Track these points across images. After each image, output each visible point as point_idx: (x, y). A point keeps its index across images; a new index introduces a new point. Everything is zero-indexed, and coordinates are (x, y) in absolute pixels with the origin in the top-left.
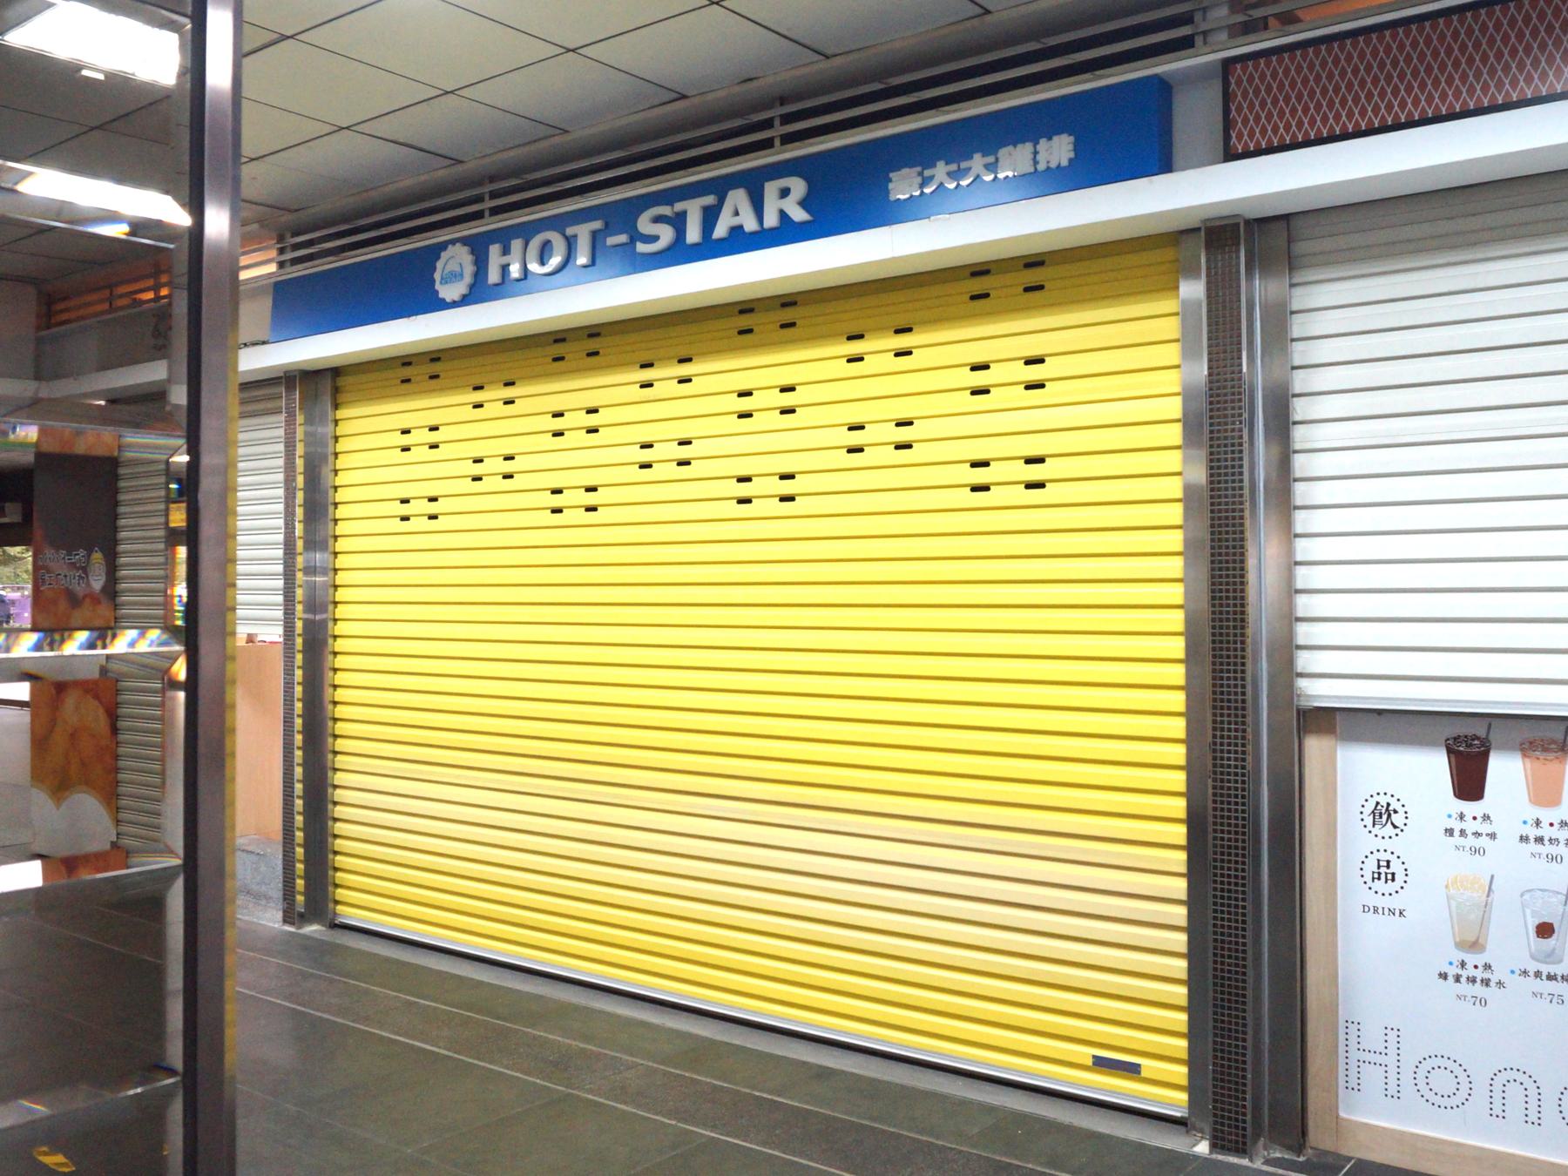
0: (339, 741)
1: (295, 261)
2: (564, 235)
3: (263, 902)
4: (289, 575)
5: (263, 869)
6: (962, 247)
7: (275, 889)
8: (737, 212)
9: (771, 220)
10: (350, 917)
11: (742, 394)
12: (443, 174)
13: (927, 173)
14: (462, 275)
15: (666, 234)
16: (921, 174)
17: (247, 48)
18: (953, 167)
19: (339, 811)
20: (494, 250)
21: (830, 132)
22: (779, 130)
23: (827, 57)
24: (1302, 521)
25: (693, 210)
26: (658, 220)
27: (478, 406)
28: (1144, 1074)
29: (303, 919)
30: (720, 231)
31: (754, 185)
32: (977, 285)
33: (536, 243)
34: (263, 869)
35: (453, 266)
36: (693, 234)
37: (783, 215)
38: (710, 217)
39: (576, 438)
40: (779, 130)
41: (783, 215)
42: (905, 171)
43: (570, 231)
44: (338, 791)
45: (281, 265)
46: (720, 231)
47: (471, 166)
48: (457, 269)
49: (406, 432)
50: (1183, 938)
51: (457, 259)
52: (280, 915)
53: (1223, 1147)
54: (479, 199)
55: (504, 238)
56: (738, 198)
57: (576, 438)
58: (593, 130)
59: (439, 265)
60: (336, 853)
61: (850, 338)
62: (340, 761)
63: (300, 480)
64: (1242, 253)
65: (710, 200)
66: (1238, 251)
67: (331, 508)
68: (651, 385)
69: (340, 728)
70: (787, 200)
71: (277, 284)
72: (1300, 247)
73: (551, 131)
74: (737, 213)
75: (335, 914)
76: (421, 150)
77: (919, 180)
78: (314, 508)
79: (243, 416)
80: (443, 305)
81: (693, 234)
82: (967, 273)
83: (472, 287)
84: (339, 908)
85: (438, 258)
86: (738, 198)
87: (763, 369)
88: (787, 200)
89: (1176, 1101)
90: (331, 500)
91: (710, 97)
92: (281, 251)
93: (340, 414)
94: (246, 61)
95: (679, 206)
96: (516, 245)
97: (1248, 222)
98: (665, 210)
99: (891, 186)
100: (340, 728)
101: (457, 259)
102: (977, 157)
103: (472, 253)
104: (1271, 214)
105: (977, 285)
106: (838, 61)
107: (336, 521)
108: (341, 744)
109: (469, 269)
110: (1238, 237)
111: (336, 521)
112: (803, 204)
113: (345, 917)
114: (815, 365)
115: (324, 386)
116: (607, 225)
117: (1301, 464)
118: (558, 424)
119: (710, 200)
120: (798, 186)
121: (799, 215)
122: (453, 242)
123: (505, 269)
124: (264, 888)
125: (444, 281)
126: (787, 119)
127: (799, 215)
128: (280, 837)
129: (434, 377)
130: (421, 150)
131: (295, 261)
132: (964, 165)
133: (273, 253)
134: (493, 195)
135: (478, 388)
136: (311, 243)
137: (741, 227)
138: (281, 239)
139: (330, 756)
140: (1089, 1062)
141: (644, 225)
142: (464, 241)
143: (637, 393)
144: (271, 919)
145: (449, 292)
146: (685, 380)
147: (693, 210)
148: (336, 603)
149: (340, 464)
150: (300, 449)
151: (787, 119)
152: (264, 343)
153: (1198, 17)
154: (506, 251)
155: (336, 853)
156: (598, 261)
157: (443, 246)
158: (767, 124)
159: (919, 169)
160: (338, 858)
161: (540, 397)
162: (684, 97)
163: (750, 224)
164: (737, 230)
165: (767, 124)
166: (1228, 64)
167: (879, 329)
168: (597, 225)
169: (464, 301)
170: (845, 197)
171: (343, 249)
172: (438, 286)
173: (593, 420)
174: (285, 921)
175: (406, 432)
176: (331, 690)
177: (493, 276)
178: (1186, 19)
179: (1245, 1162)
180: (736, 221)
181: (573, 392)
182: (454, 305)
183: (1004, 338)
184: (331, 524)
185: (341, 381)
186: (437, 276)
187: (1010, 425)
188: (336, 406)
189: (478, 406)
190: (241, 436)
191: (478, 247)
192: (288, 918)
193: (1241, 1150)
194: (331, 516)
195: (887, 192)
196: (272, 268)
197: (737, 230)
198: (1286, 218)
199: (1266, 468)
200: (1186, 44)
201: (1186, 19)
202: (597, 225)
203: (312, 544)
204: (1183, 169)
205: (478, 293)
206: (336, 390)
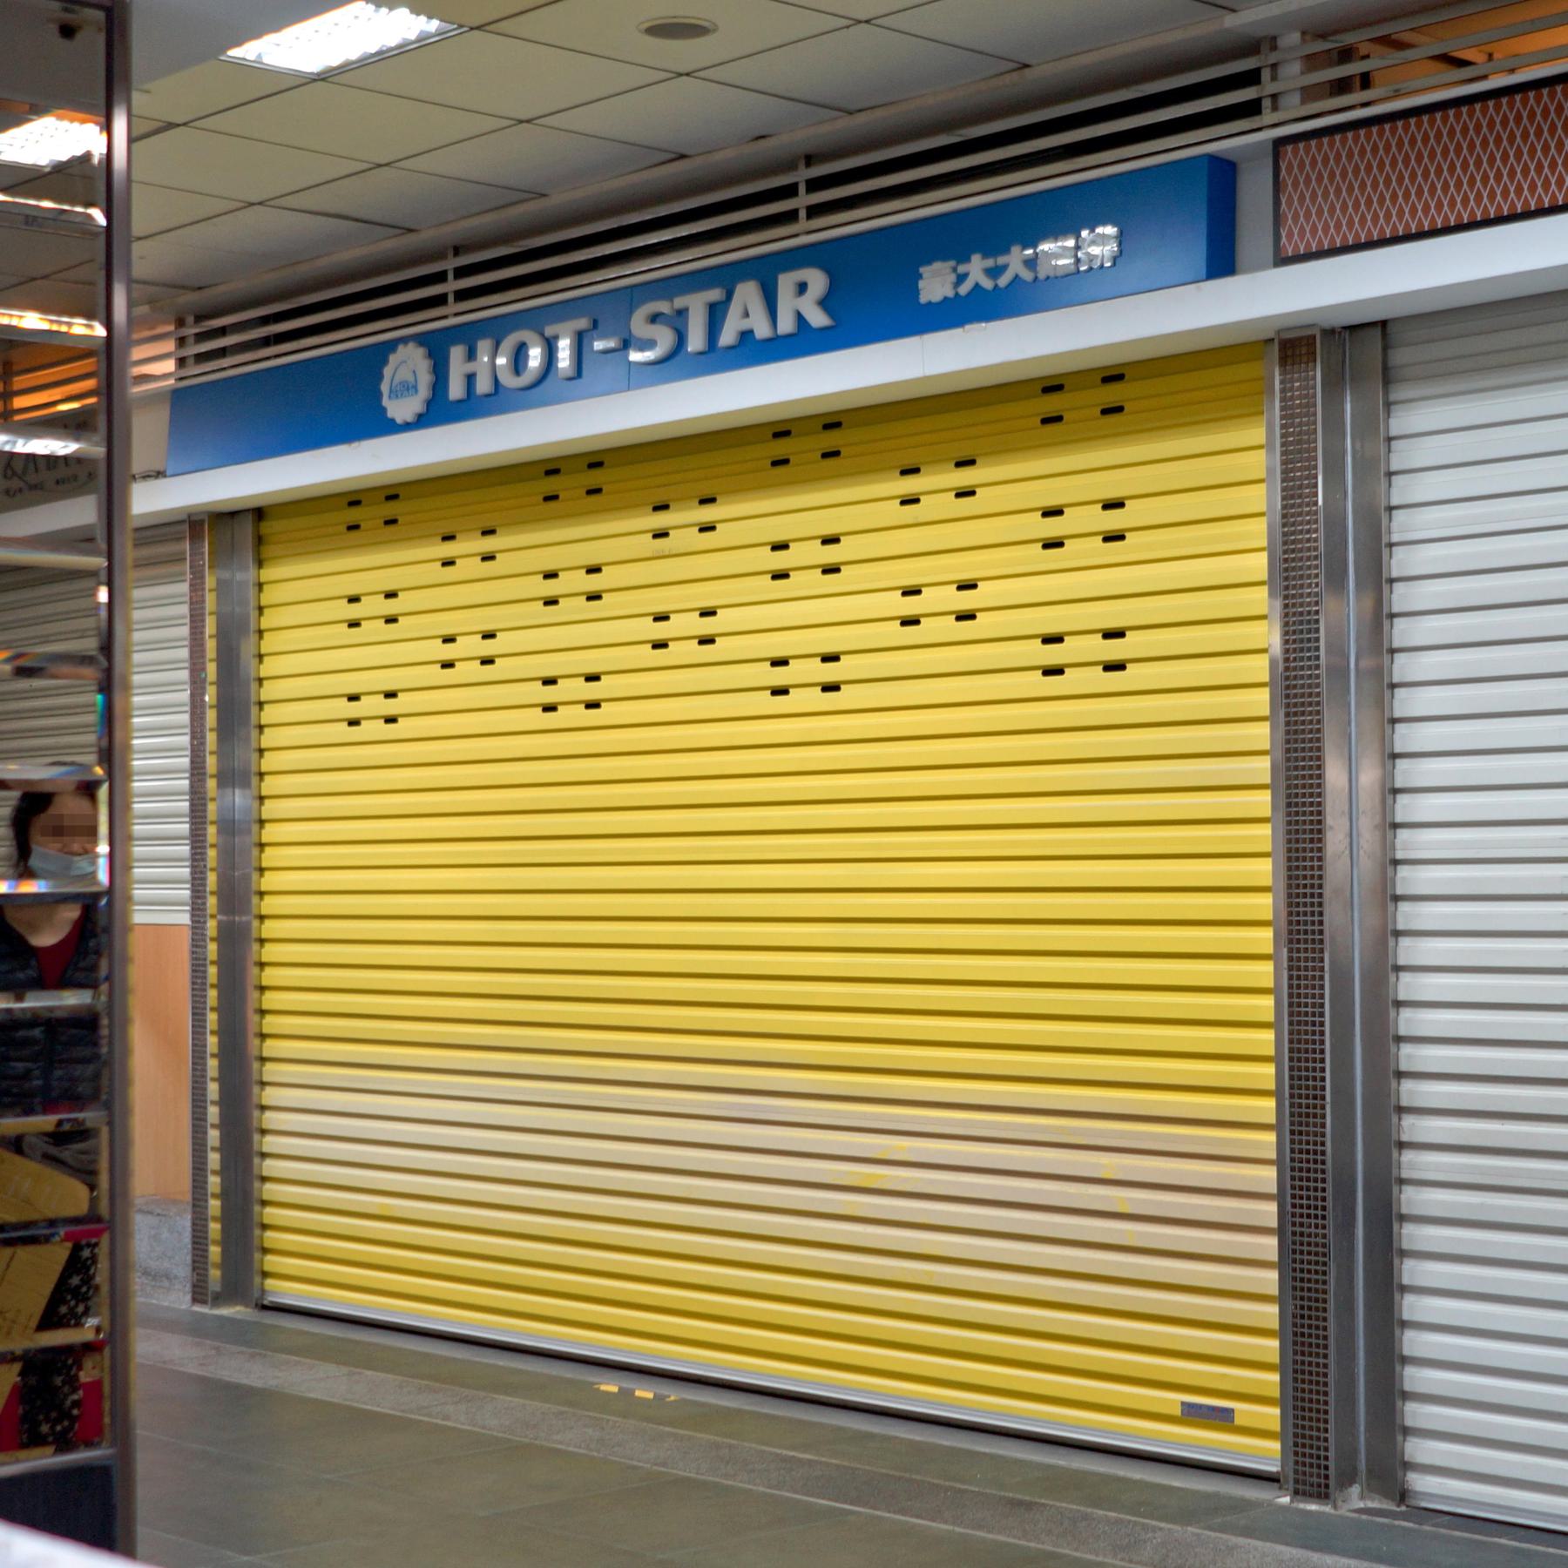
0: (269, 1042)
1: (201, 358)
2: (542, 335)
3: (166, 1283)
4: (197, 814)
5: (165, 1235)
6: (997, 365)
7: (182, 1267)
8: (747, 312)
9: (786, 325)
10: (284, 1295)
11: (1110, 505)
12: (391, 245)
13: (962, 269)
14: (415, 387)
15: (665, 339)
16: (955, 270)
17: (134, 134)
18: (990, 263)
19: (270, 1167)
20: (457, 353)
21: (867, 201)
22: (803, 200)
23: (850, 113)
24: (1406, 703)
25: (696, 305)
26: (654, 318)
27: (448, 563)
28: (1238, 1421)
29: (218, 1300)
30: (727, 337)
31: (765, 274)
32: (1052, 404)
33: (509, 343)
34: (165, 1235)
35: (404, 375)
36: (696, 341)
37: (800, 318)
38: (716, 315)
39: (572, 607)
40: (803, 200)
41: (800, 318)
42: (937, 265)
43: (549, 331)
44: (268, 1114)
45: (181, 362)
46: (727, 337)
47: (427, 236)
48: (411, 379)
49: (551, 575)
50: (1272, 1242)
51: (409, 364)
52: (188, 1297)
53: (1304, 1494)
54: (440, 277)
55: (468, 336)
56: (748, 293)
57: (572, 607)
58: (579, 194)
59: (387, 371)
60: (264, 1203)
61: (959, 464)
62: (271, 1071)
63: (211, 670)
64: (1350, 361)
65: (715, 295)
66: (1314, 369)
67: (254, 710)
68: (713, 528)
69: (271, 1023)
70: (804, 298)
71: (175, 393)
72: (1399, 357)
73: (526, 196)
74: (747, 315)
75: (263, 1291)
76: (357, 220)
77: (953, 278)
78: (231, 710)
79: (138, 565)
80: (392, 427)
81: (696, 341)
82: (1039, 387)
83: (429, 403)
84: (270, 1283)
85: (385, 362)
86: (748, 293)
87: (801, 511)
88: (804, 298)
89: (1268, 1453)
90: (253, 699)
91: (718, 157)
92: (181, 342)
93: (267, 574)
94: (135, 146)
95: (679, 302)
96: (484, 346)
97: (1330, 333)
98: (663, 307)
99: (921, 284)
100: (271, 1023)
101: (409, 364)
102: (1015, 250)
103: (430, 355)
104: (1428, 309)
105: (1052, 404)
106: (861, 119)
107: (261, 728)
108: (271, 1047)
109: (425, 379)
110: (1314, 353)
111: (261, 728)
112: (823, 303)
113: (275, 1293)
114: (860, 505)
115: (246, 531)
116: (595, 324)
117: (1403, 632)
118: (780, 560)
119: (715, 295)
120: (817, 281)
121: (818, 319)
122: (404, 340)
123: (470, 379)
124: (166, 1264)
125: (394, 394)
126: (814, 185)
127: (818, 319)
128: (188, 1197)
129: (391, 522)
130: (357, 220)
131: (201, 358)
132: (1001, 260)
133: (169, 346)
134: (461, 272)
135: (448, 538)
136: (222, 331)
137: (751, 332)
138: (180, 323)
139: (256, 1065)
140: (1177, 1411)
141: (638, 325)
142: (421, 339)
143: (648, 544)
144: (178, 1299)
145: (401, 409)
146: (707, 528)
147: (696, 305)
148: (262, 846)
149: (266, 647)
150: (210, 626)
151: (814, 185)
152: (159, 474)
153: (1266, 75)
154: (471, 355)
155: (264, 1203)
156: (585, 373)
157: (392, 346)
158: (790, 191)
159: (952, 263)
160: (268, 1210)
161: (531, 547)
162: (682, 157)
163: (762, 330)
164: (746, 335)
165: (790, 191)
166: (1279, 143)
167: (936, 461)
168: (582, 323)
169: (422, 421)
170: (873, 299)
171: (266, 342)
172: (385, 402)
173: (831, 554)
174: (195, 1300)
175: (551, 575)
176: (256, 970)
177: (456, 390)
178: (1252, 78)
179: (1327, 1509)
180: (745, 325)
181: (567, 542)
182: (407, 427)
183: (1078, 472)
184: (254, 733)
185: (267, 527)
186: (385, 388)
187: (1085, 585)
188: (260, 564)
189: (448, 563)
190: (137, 594)
191: (436, 348)
192: (199, 1293)
193: (1322, 1495)
194: (254, 721)
195: (917, 291)
196: (172, 381)
197: (746, 335)
198: (1383, 324)
199: (1357, 640)
200: (1251, 109)
201: (1252, 78)
202: (582, 323)
203: (232, 777)
204: (1246, 271)
205: (438, 411)
206: (259, 540)
